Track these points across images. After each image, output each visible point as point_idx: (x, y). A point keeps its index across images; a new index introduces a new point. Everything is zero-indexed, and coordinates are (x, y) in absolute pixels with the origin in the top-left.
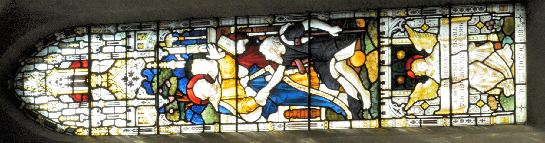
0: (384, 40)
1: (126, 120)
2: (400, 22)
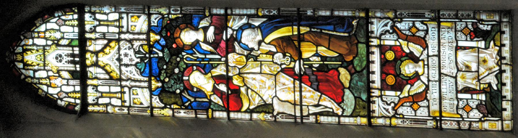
0: (372, 40)
2: (388, 23)
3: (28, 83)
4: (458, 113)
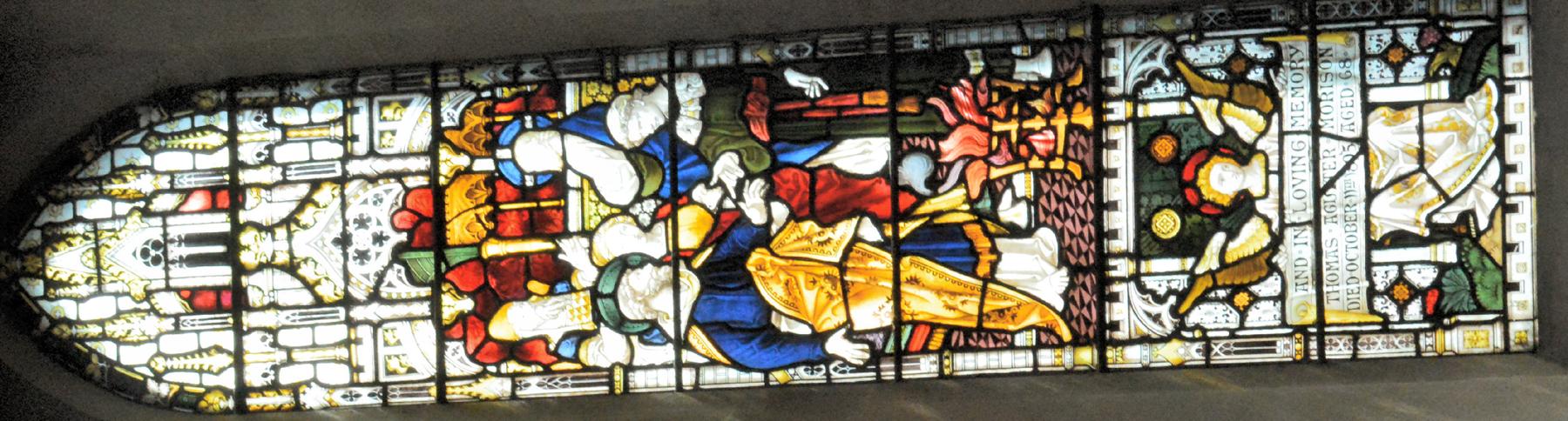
1: (348, 362)
2: (1157, 49)
3: (59, 339)
4: (1372, 311)
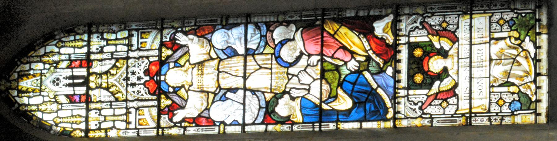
1: (126, 121)
